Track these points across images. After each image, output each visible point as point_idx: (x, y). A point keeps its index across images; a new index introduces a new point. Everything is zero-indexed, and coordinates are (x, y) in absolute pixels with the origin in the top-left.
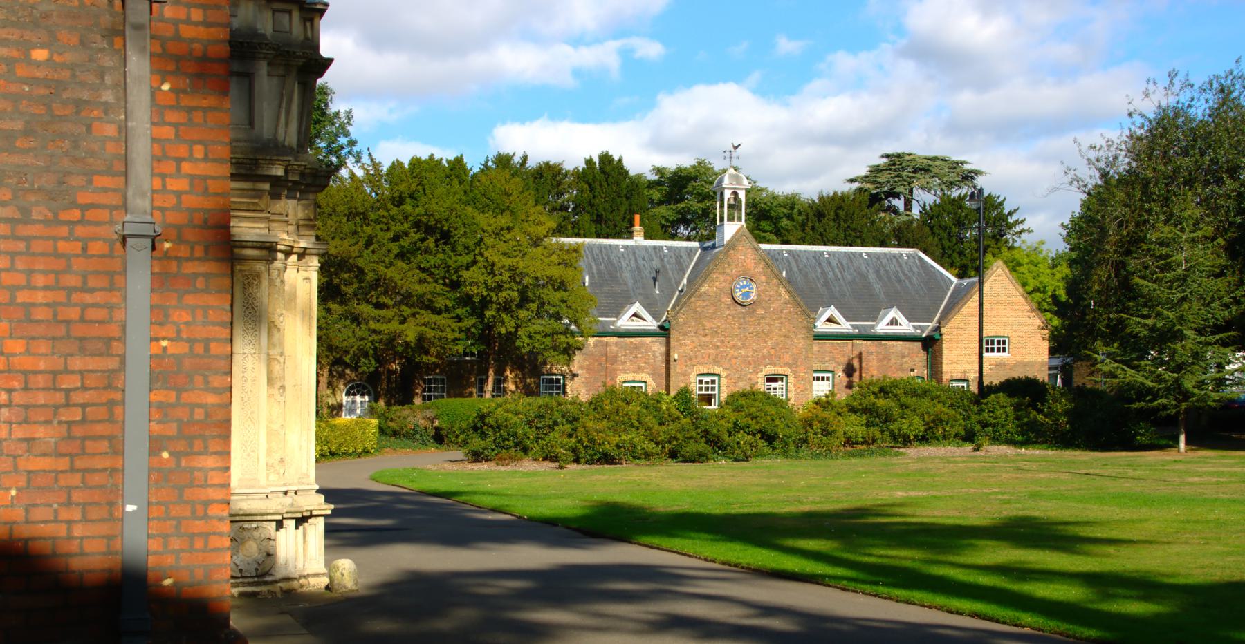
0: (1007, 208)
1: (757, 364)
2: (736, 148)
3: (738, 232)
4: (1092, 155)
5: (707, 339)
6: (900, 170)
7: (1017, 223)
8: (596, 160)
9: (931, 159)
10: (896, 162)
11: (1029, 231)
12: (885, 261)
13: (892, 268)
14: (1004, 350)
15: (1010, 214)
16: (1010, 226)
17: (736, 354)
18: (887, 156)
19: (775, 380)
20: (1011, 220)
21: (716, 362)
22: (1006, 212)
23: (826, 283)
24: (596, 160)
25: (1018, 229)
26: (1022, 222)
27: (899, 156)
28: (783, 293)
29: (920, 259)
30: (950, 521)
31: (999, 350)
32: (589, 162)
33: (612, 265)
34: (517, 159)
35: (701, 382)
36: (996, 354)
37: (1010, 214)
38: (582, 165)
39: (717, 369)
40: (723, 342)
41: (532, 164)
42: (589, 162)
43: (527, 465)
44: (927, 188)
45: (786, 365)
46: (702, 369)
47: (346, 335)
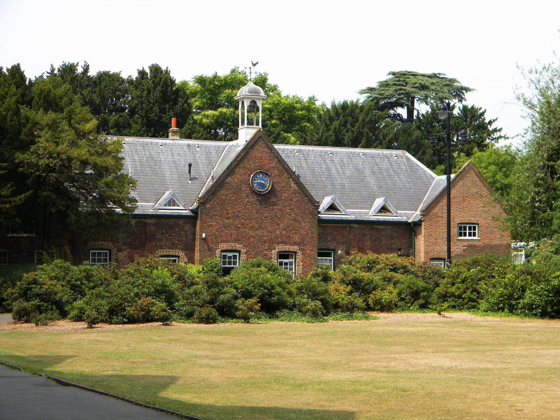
0: (488, 118)
1: (271, 243)
2: (254, 65)
3: (256, 134)
4: (534, 76)
5: (230, 221)
6: (404, 87)
7: (495, 130)
8: (148, 71)
9: (430, 77)
10: (401, 78)
11: (506, 138)
12: (378, 160)
13: (385, 165)
14: (474, 235)
15: (490, 123)
16: (489, 134)
17: (253, 234)
18: (394, 74)
19: (287, 257)
20: (491, 128)
21: (237, 241)
22: (487, 121)
23: (330, 176)
24: (148, 71)
25: (497, 135)
26: (500, 130)
27: (403, 74)
28: (293, 185)
29: (408, 159)
30: (295, 407)
31: (470, 235)
32: (142, 73)
33: (153, 159)
34: (80, 70)
35: (225, 257)
36: (467, 237)
37: (490, 123)
38: (135, 76)
39: (238, 246)
40: (243, 224)
41: (93, 73)
42: (142, 73)
43: (65, 325)
44: (425, 100)
45: (295, 244)
46: (224, 246)
47: (427, 157)
